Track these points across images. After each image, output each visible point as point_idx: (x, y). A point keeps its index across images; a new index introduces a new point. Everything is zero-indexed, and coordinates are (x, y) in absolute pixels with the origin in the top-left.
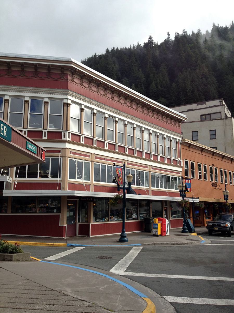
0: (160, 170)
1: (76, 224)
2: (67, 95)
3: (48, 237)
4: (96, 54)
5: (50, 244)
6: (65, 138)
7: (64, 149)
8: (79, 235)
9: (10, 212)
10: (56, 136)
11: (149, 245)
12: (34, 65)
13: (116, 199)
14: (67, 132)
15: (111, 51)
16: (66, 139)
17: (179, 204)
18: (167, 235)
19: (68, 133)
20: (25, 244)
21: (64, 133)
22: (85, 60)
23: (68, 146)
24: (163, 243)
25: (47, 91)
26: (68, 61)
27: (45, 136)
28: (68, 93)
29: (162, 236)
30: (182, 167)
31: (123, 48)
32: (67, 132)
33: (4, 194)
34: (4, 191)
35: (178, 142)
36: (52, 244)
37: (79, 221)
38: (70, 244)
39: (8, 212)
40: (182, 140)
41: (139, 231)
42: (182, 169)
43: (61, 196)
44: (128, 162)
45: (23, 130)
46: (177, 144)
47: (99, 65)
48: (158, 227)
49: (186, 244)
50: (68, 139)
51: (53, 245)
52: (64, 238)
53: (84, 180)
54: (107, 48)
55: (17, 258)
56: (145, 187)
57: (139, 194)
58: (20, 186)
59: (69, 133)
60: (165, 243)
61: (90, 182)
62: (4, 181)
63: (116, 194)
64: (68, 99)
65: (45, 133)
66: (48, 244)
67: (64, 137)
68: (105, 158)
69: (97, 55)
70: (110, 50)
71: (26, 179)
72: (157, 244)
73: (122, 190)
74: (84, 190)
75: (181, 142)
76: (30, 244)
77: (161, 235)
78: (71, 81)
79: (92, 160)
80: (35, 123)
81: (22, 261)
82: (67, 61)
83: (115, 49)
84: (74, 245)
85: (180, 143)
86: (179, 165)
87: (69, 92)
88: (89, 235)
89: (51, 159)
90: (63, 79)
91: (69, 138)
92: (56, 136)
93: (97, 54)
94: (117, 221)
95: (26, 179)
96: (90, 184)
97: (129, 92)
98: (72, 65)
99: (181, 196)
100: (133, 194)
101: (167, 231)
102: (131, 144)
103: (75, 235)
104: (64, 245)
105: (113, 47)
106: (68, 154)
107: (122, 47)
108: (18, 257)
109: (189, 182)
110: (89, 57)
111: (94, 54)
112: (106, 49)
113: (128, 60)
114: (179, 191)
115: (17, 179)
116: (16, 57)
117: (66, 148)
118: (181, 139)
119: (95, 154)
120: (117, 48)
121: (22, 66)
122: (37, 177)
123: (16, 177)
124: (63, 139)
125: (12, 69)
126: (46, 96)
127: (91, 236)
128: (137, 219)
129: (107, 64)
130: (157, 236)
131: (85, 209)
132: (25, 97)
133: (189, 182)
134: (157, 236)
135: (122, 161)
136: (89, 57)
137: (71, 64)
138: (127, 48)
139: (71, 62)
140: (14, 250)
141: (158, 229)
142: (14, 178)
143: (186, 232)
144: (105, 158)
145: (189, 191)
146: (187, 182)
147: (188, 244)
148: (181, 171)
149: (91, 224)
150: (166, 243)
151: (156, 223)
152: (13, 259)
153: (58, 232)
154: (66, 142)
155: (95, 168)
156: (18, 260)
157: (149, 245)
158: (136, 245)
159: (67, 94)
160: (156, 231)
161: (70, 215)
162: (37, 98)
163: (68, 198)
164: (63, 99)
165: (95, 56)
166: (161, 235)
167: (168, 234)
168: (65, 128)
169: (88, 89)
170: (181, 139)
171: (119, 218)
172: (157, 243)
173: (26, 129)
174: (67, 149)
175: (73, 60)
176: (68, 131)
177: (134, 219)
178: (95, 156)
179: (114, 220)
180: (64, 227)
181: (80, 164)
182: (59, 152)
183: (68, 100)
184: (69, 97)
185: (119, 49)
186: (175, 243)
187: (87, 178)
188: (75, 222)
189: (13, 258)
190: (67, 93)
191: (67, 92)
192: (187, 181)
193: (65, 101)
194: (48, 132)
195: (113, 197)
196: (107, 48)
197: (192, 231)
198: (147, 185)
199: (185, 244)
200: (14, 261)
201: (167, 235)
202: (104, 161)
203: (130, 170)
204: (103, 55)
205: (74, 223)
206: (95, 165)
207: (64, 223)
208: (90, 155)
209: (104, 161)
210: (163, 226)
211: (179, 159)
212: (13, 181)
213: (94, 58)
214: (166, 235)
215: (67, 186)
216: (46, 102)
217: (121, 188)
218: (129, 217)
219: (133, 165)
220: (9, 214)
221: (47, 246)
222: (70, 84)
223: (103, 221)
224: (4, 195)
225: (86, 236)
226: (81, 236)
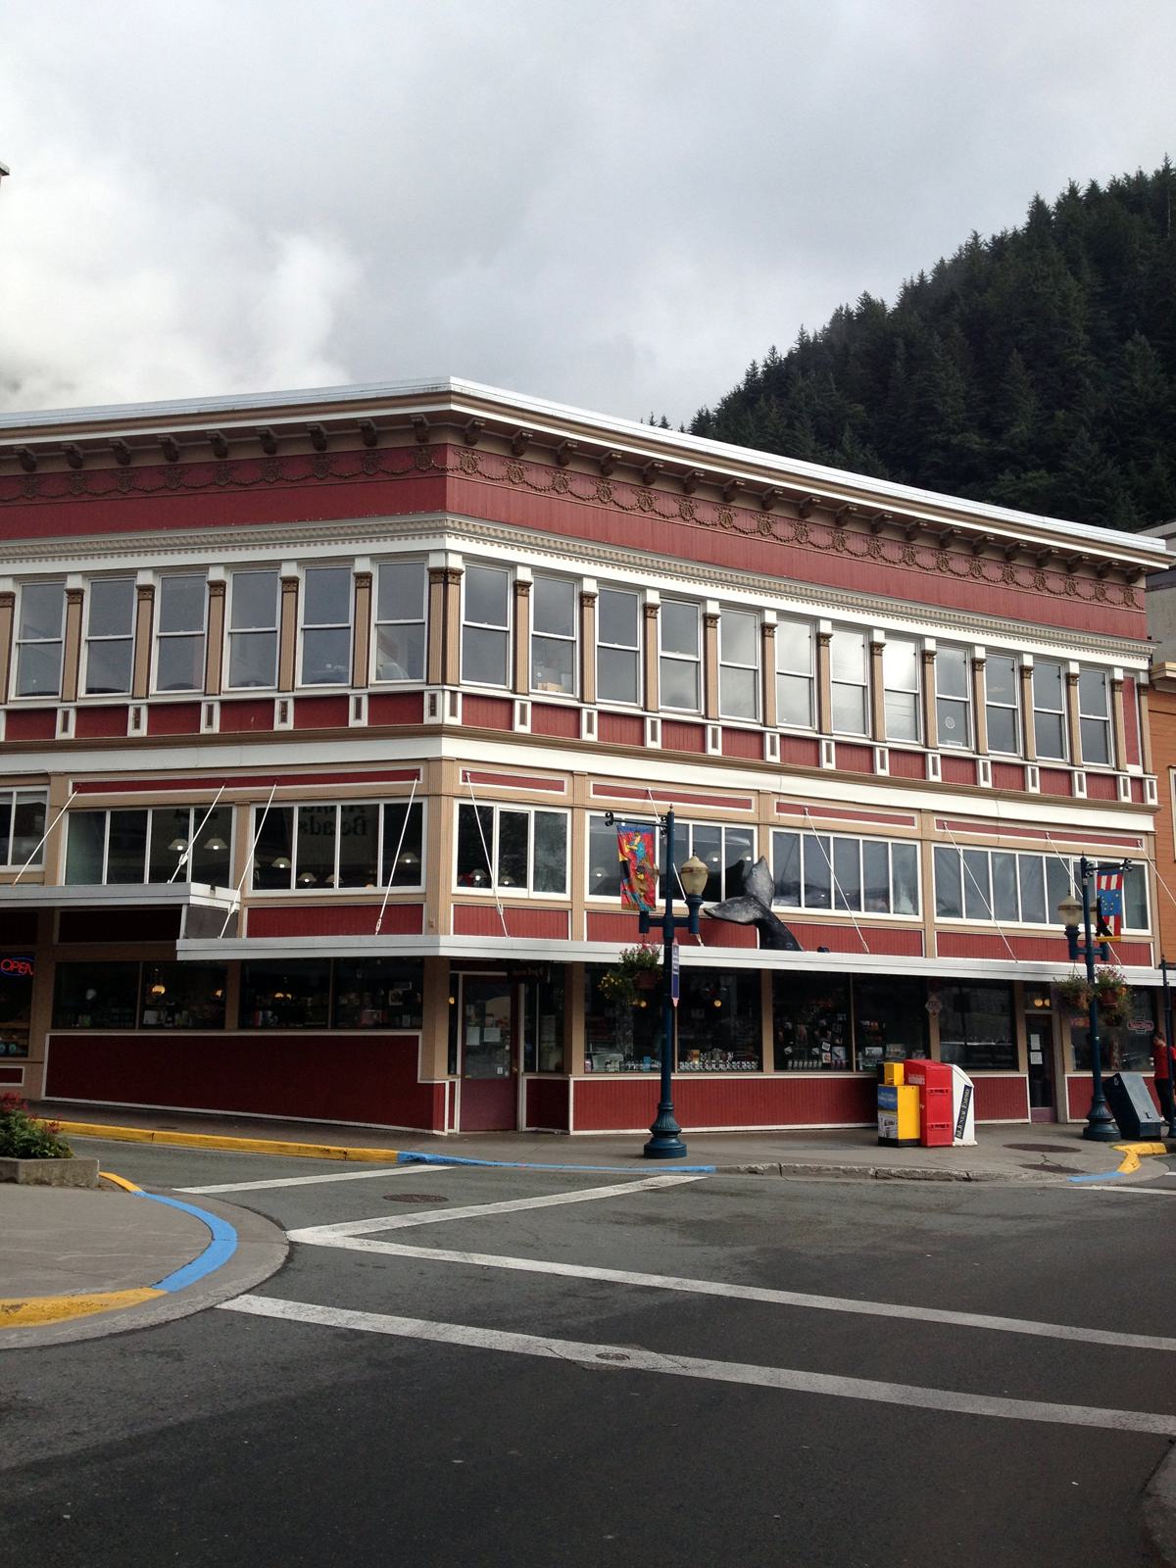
0: (997, 830)
1: (514, 1078)
2: (441, 535)
3: (373, 1125)
4: (976, 237)
5: (335, 1151)
6: (434, 718)
7: (431, 763)
8: (527, 1126)
9: (236, 1026)
10: (400, 712)
11: (756, 1173)
12: (259, 433)
13: (629, 967)
14: (443, 690)
15: (1059, 205)
16: (440, 722)
17: (1064, 996)
18: (957, 1142)
19: (447, 694)
20: (243, 1147)
21: (433, 697)
22: (922, 276)
23: (450, 747)
24: (829, 1170)
25: (363, 531)
26: (435, 391)
27: (358, 716)
28: (448, 527)
29: (926, 1146)
30: (1151, 811)
31: (1127, 177)
32: (443, 690)
33: (183, 953)
34: (180, 943)
35: (1120, 683)
36: (340, 1151)
37: (530, 1068)
38: (409, 1154)
39: (226, 1027)
40: (1149, 672)
41: (852, 1122)
42: (1155, 820)
43: (759, 970)
44: (784, 800)
45: (205, 701)
46: (1113, 691)
47: (989, 290)
48: (896, 1102)
49: (957, 1179)
50: (449, 720)
51: (345, 1153)
52: (435, 1132)
53: (535, 889)
54: (1037, 198)
55: (39, 1174)
56: (891, 916)
57: (820, 950)
58: (264, 921)
59: (453, 693)
60: (839, 1169)
61: (565, 897)
62: (181, 905)
63: (632, 947)
64: (446, 552)
65: (284, 705)
66: (328, 1150)
67: (433, 713)
68: (647, 791)
69: (981, 240)
70: (1051, 202)
71: (337, 890)
72: (795, 1171)
73: (661, 929)
74: (497, 931)
75: (1143, 679)
76: (263, 1146)
77: (920, 1143)
78: (463, 473)
79: (578, 802)
80: (329, 666)
81: (61, 1185)
82: (430, 391)
83: (1081, 194)
84: (427, 1157)
85: (1140, 687)
86: (1127, 799)
87: (451, 520)
88: (567, 1127)
89: (385, 805)
90: (425, 471)
91: (453, 713)
92: (400, 712)
93: (986, 238)
94: (721, 1071)
95: (337, 890)
96: (569, 906)
97: (771, 473)
98: (454, 407)
99: (1073, 957)
100: (784, 948)
101: (962, 1122)
102: (808, 720)
103: (514, 1125)
104: (387, 1157)
105: (1125, 174)
106: (453, 781)
107: (1120, 176)
108: (41, 1169)
109: (1113, 886)
110: (942, 261)
111: (965, 239)
112: (1032, 199)
113: (1153, 237)
114: (1066, 933)
115: (389, 890)
116: (236, 408)
117: (440, 760)
118: (1144, 665)
119: (590, 774)
120: (1094, 186)
121: (268, 440)
122: (288, 886)
123: (385, 884)
124: (428, 720)
125: (187, 459)
126: (362, 548)
127: (573, 1133)
128: (848, 1067)
129: (1031, 280)
130: (894, 1143)
131: (553, 1017)
132: (211, 570)
133: (1113, 886)
134: (894, 1143)
135: (748, 797)
136: (942, 261)
137: (449, 401)
138: (1150, 174)
139: (448, 395)
140: (38, 1148)
141: (897, 1110)
142: (251, 892)
143: (1105, 1138)
144: (650, 789)
145: (1112, 931)
146: (1103, 886)
147: (968, 1179)
148: (1146, 833)
149: (572, 1080)
150: (841, 1167)
151: (892, 1083)
152: (22, 1176)
153: (416, 1110)
154: (438, 731)
155: (591, 835)
156: (40, 1182)
157: (753, 1172)
158: (688, 1168)
159: (440, 531)
160: (892, 1123)
161: (486, 1040)
162: (331, 561)
163: (451, 969)
164: (425, 554)
165: (973, 248)
166: (920, 1143)
167: (969, 1136)
168: (437, 677)
169: (554, 495)
170: (1144, 665)
171: (734, 1059)
172: (797, 1165)
173: (286, 694)
174: (444, 763)
175: (457, 384)
176: (446, 687)
177: (826, 1067)
178: (593, 782)
179: (707, 1067)
180: (435, 1089)
181: (514, 825)
182: (414, 775)
183: (446, 554)
184: (451, 543)
185: (1104, 186)
186: (892, 1171)
187: (552, 878)
188: (511, 1071)
189: (20, 1174)
190: (439, 525)
191: (440, 521)
192: (1104, 879)
193: (435, 562)
194: (371, 696)
195: (617, 959)
196: (1037, 198)
197: (1141, 1135)
198: (905, 903)
199: (949, 1180)
200: (22, 1183)
201: (957, 1142)
202: (644, 803)
203: (828, 838)
204: (1015, 233)
205: (507, 1074)
206: (591, 824)
207: (437, 1070)
208: (566, 779)
209: (643, 801)
210: (932, 1100)
211: (1135, 770)
212: (244, 900)
213: (969, 258)
214: (954, 1144)
215: (449, 917)
216: (360, 573)
217: (656, 922)
218: (797, 1056)
219: (815, 811)
220: (230, 1030)
221: (322, 1156)
222: (456, 486)
223: (640, 1071)
224: (180, 957)
225: (556, 1131)
226: (540, 1129)
